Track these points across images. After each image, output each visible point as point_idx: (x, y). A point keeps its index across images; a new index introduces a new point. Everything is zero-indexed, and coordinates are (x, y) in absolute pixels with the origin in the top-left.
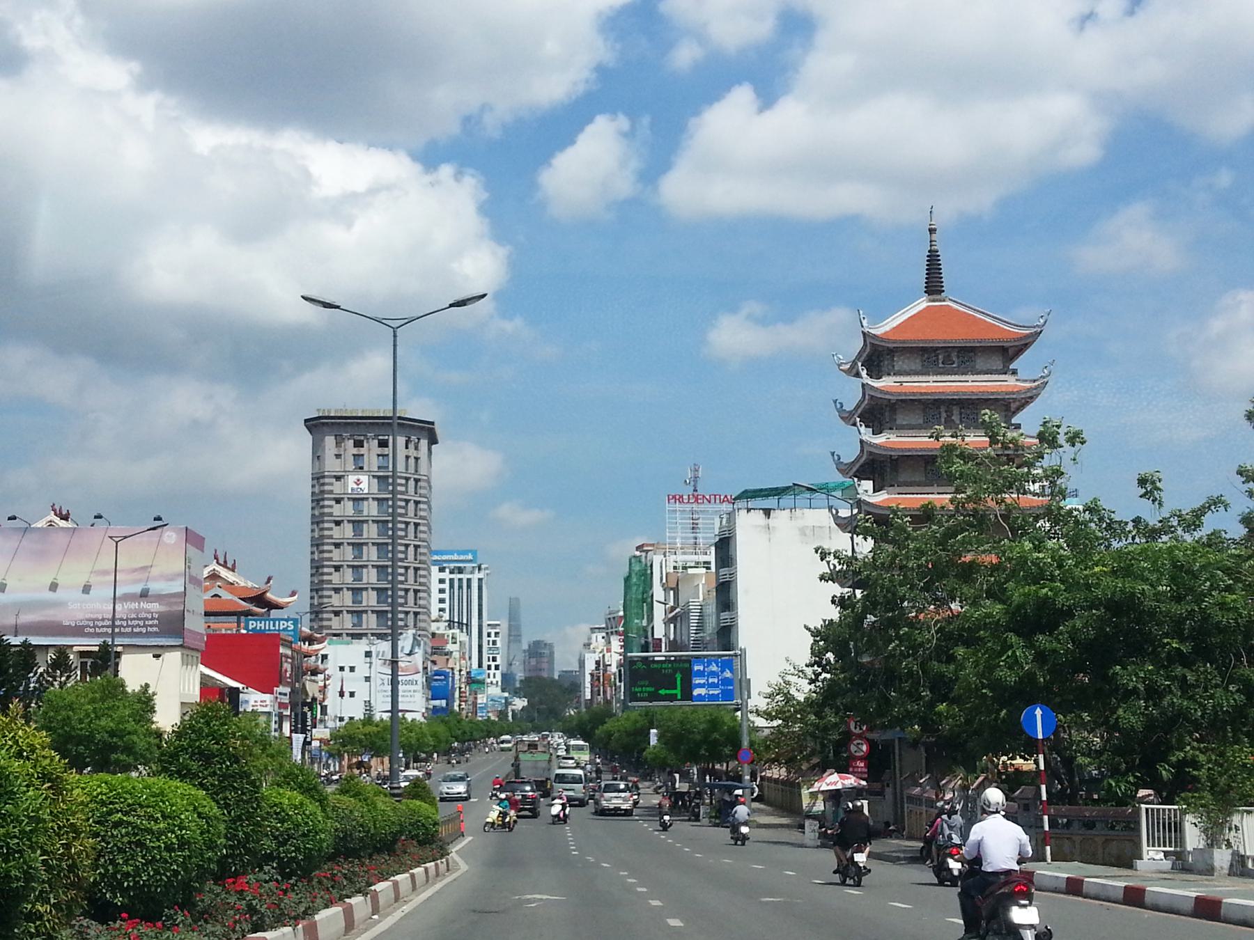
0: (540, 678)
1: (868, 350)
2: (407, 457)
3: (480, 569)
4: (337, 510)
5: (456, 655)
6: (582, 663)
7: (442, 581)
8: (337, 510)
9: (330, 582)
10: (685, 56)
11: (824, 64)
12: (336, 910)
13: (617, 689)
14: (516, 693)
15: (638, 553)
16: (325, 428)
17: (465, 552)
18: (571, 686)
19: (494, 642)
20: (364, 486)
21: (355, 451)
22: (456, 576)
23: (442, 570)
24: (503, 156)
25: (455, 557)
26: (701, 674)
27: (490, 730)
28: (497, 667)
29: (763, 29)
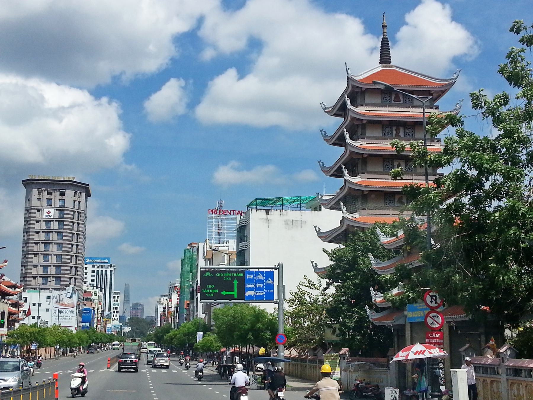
0: (138, 318)
1: (350, 89)
2: (75, 201)
3: (111, 266)
4: (37, 226)
5: (96, 301)
6: (156, 310)
8: (37, 226)
9: (31, 262)
10: (208, 54)
11: (266, 61)
13: (175, 317)
14: (126, 324)
15: (189, 247)
16: (33, 185)
17: (105, 259)
18: (151, 322)
19: (117, 301)
20: (52, 214)
21: (48, 197)
22: (100, 269)
23: (93, 266)
24: (128, 94)
25: (99, 261)
26: (251, 281)
27: (111, 338)
28: (117, 312)
29: (240, 44)
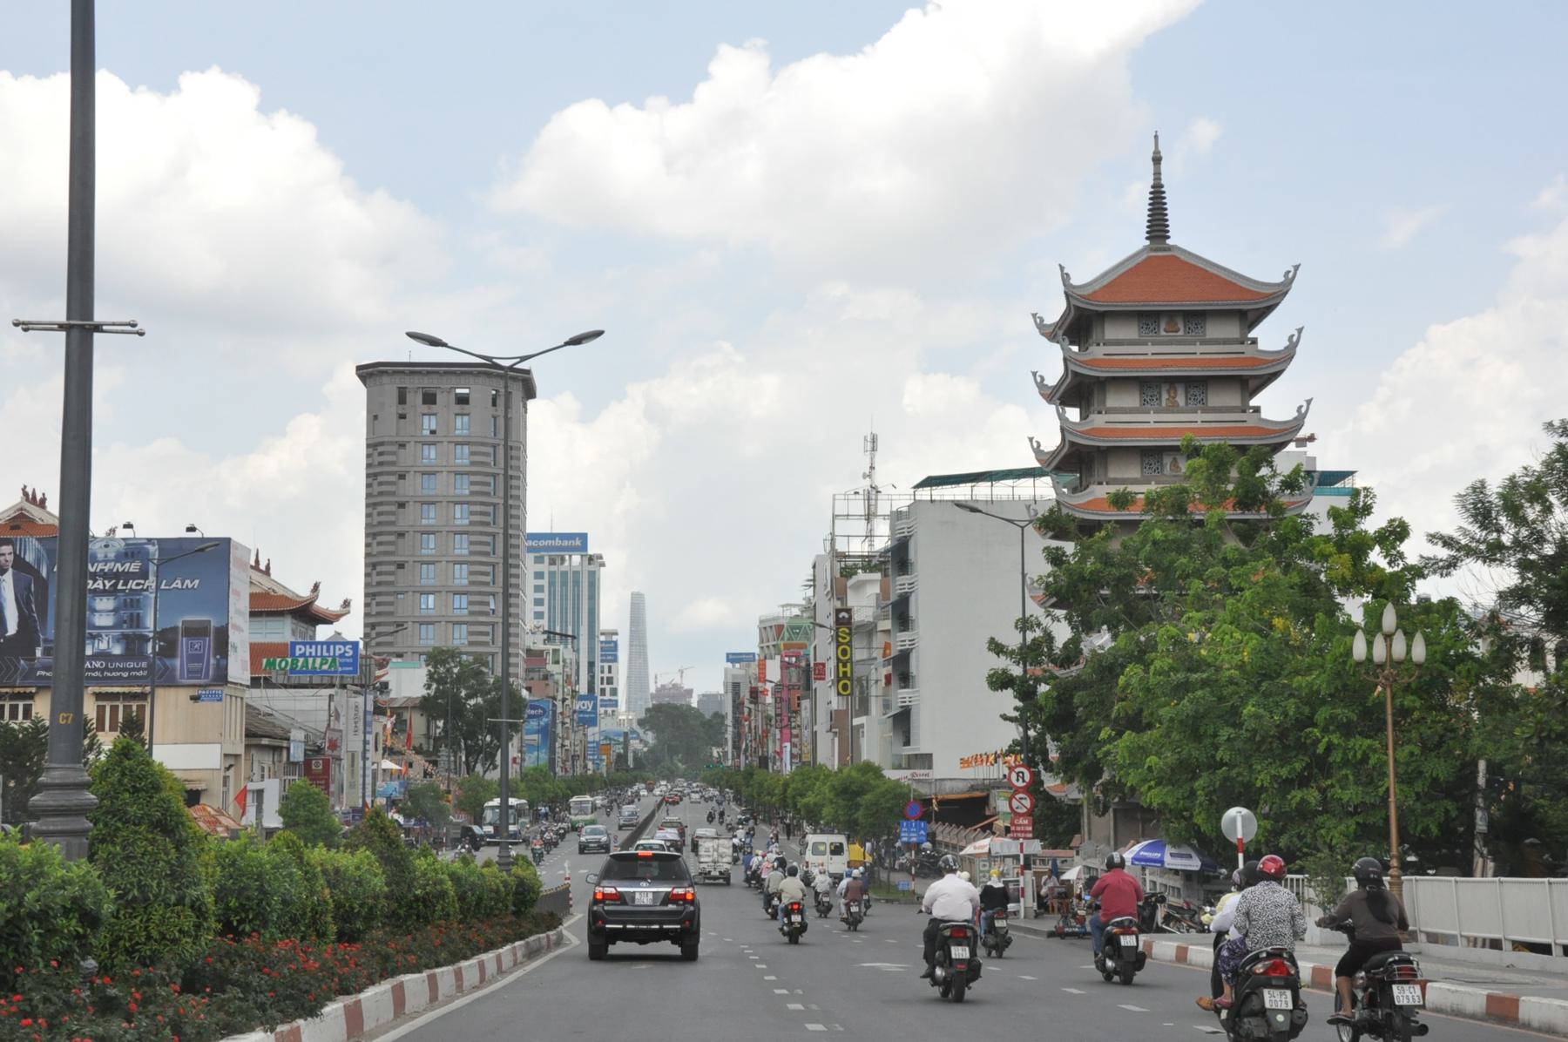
7: (539, 575)
12: (385, 986)
23: (539, 560)
